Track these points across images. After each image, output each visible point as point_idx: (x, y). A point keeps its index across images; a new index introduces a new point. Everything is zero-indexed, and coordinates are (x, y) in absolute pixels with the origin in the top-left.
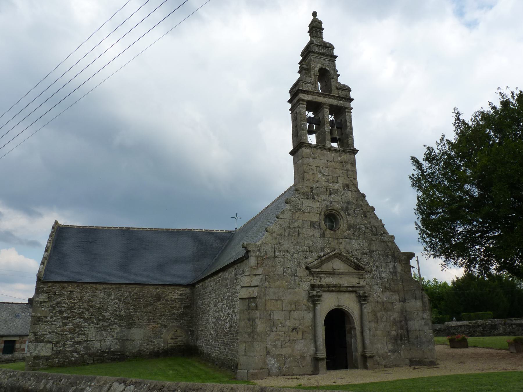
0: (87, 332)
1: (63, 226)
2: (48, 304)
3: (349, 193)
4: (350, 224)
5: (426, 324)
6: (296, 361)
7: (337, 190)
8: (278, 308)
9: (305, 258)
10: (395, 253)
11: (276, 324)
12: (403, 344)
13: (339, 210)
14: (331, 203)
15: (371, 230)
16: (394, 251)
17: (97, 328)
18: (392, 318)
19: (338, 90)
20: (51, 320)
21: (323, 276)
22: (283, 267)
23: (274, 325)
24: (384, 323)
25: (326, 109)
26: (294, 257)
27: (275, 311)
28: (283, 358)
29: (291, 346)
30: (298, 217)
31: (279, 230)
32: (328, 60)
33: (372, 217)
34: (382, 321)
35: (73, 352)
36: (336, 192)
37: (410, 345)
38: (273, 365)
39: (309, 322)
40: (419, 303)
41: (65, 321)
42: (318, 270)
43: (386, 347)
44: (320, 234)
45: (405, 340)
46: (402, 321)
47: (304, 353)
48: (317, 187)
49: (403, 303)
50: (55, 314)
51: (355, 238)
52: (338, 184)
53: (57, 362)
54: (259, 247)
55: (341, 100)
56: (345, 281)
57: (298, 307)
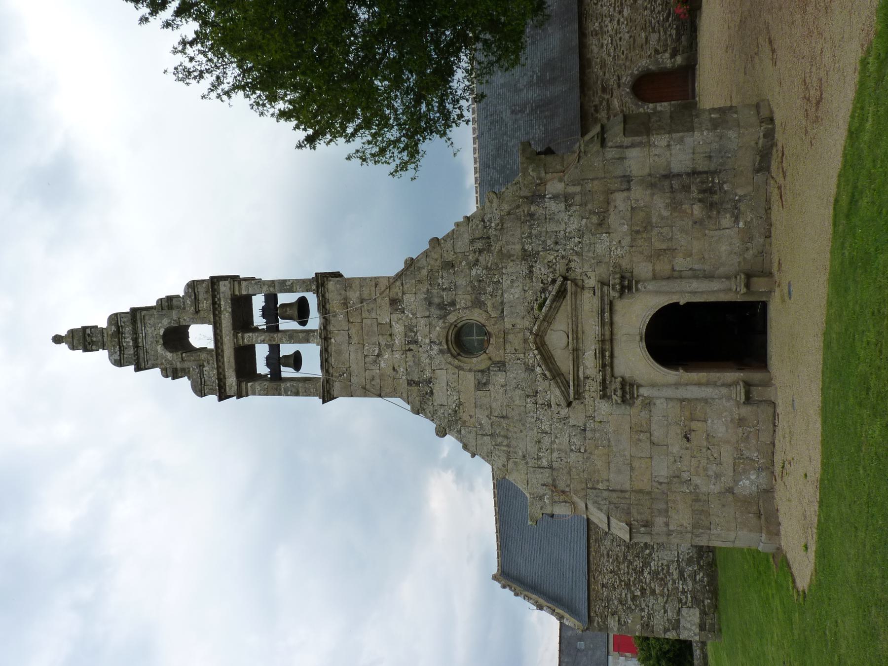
0: (665, 563)
1: (500, 568)
2: (623, 616)
3: (409, 299)
4: (471, 302)
5: (681, 141)
6: (748, 437)
7: (405, 326)
8: (647, 468)
9: (550, 406)
10: (524, 195)
11: (676, 473)
12: (721, 188)
13: (447, 324)
14: (434, 343)
15: (481, 251)
16: (521, 197)
17: (658, 549)
18: (666, 213)
19: (199, 310)
20: (646, 611)
21: (582, 373)
22: (568, 453)
23: (678, 477)
24: (676, 235)
25: (245, 340)
26: (548, 430)
27: (652, 473)
28: (741, 463)
29: (718, 445)
30: (471, 416)
31: (499, 456)
32: (143, 328)
33: (452, 249)
34: (671, 239)
35: (694, 581)
36: (412, 331)
37: (724, 170)
38: (752, 483)
39: (673, 407)
40: (634, 153)
41: (648, 592)
42: (571, 384)
43: (727, 230)
44: (500, 370)
45: (713, 182)
46: (672, 187)
47: (732, 420)
48: (405, 372)
49: (632, 180)
50: (636, 606)
51: (500, 292)
52: (393, 324)
53: (709, 601)
54: (534, 498)
55: (220, 305)
56: (592, 328)
57: (645, 426)
